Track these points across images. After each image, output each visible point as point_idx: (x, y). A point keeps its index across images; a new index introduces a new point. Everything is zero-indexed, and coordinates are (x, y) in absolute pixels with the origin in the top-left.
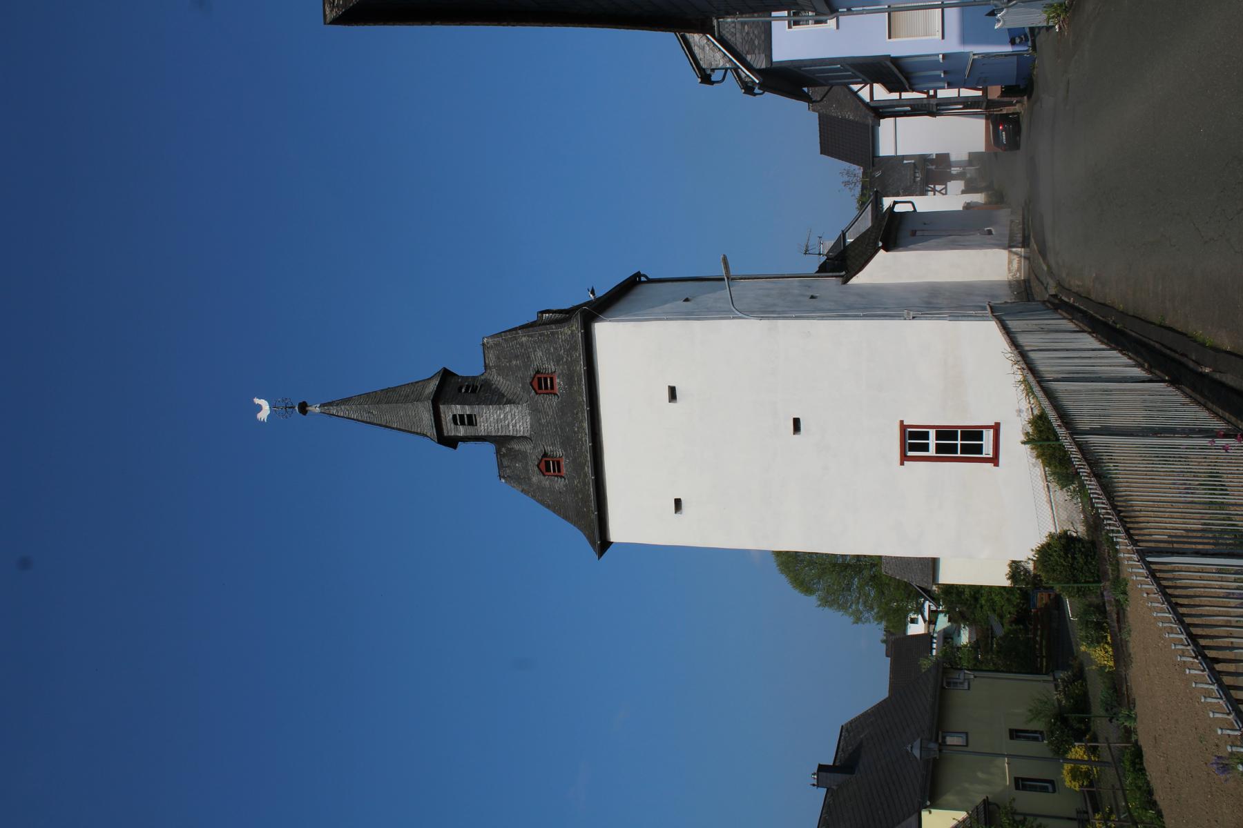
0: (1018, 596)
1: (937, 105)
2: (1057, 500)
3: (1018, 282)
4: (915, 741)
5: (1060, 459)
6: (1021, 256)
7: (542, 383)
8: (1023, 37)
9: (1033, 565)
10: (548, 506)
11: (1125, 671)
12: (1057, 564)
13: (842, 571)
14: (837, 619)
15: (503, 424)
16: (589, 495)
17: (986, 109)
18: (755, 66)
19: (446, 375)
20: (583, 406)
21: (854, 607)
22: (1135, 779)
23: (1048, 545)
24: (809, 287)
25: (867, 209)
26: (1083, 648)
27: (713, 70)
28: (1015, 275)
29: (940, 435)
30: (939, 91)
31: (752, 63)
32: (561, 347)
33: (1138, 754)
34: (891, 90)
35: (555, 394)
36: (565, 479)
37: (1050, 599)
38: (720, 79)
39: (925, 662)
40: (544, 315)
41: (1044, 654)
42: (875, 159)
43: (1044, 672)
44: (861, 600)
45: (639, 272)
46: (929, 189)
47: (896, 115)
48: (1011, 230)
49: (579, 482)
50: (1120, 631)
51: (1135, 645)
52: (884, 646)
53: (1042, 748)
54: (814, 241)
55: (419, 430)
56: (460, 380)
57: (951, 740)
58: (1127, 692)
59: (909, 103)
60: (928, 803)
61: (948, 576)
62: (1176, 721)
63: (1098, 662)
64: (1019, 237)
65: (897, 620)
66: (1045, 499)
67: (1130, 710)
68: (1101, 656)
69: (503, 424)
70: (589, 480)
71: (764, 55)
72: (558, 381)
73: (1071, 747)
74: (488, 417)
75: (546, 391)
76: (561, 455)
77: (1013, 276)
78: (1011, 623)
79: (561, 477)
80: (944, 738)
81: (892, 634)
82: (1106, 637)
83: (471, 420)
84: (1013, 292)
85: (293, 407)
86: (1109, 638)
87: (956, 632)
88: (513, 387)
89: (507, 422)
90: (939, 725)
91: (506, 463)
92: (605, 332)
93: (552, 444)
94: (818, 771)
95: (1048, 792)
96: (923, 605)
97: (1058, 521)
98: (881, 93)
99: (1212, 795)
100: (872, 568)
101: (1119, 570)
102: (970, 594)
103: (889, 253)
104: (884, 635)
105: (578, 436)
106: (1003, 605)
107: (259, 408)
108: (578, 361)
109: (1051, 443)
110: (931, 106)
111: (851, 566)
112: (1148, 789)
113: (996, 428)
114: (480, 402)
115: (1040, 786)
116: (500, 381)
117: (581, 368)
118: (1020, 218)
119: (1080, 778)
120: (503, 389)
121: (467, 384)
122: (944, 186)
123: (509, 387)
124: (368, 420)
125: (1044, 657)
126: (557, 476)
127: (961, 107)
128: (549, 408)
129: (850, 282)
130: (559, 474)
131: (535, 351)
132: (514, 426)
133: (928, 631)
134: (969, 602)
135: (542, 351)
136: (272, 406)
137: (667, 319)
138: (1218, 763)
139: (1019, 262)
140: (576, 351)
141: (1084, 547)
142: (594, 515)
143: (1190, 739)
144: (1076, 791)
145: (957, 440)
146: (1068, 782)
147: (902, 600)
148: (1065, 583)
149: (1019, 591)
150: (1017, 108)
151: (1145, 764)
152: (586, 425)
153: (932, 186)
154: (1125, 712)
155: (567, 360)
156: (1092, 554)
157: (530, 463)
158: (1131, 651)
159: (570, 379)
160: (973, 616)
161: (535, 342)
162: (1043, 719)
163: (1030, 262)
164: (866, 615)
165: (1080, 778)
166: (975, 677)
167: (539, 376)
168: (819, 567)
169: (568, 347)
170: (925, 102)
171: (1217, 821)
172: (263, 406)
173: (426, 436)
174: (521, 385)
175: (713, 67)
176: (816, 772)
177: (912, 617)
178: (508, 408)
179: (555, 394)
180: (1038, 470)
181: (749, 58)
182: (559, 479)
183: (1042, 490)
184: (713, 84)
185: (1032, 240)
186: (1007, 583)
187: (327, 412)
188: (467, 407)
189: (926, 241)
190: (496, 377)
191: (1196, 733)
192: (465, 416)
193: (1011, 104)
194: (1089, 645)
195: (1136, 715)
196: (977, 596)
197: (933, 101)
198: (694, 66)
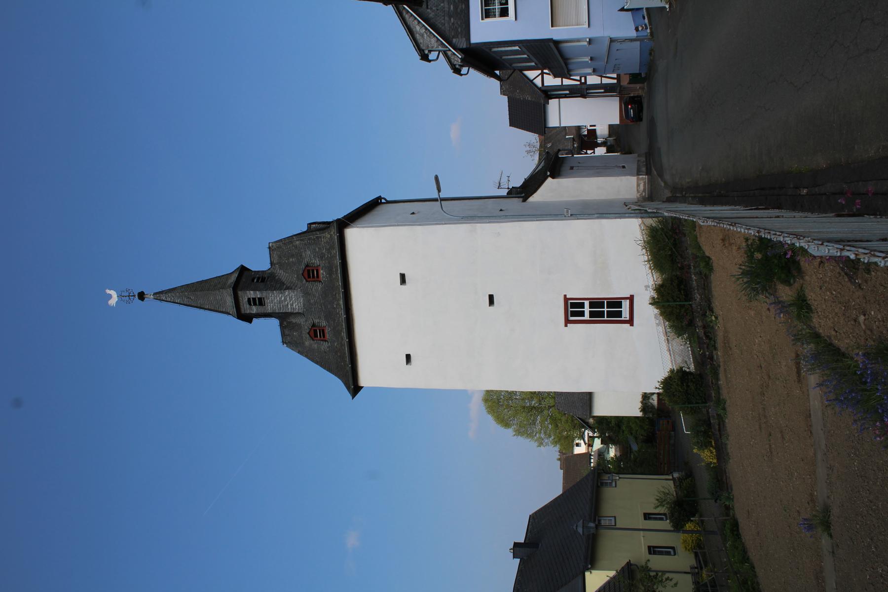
4: (579, 521)
7: (310, 274)
8: (643, 26)
10: (317, 363)
14: (526, 444)
15: (284, 304)
16: (345, 353)
19: (243, 270)
21: (538, 436)
26: (695, 451)
27: (430, 51)
29: (592, 305)
30: (588, 77)
32: (323, 247)
33: (735, 526)
34: (555, 76)
35: (320, 281)
45: (380, 196)
47: (559, 97)
50: (721, 437)
51: (732, 445)
55: (224, 310)
56: (253, 273)
58: (726, 480)
60: (590, 566)
63: (706, 460)
65: (567, 443)
66: (666, 349)
68: (707, 456)
70: (344, 343)
72: (322, 271)
77: (640, 195)
79: (325, 341)
81: (564, 454)
82: (711, 442)
83: (261, 302)
85: (134, 296)
86: (713, 442)
87: (607, 450)
88: (290, 277)
91: (287, 332)
93: (319, 318)
94: (514, 547)
95: (671, 555)
100: (549, 409)
104: (559, 455)
108: (336, 257)
109: (671, 304)
111: (535, 408)
113: (631, 299)
115: (665, 551)
117: (338, 261)
120: (284, 279)
122: (593, 151)
123: (288, 278)
124: (188, 304)
126: (322, 340)
127: (603, 91)
128: (316, 292)
130: (324, 339)
132: (292, 305)
134: (614, 429)
136: (120, 296)
138: (805, 524)
141: (694, 378)
147: (570, 430)
149: (647, 420)
152: (341, 302)
153: (585, 151)
154: (725, 494)
155: (328, 256)
156: (700, 383)
159: (330, 270)
166: (620, 478)
167: (308, 268)
169: (328, 247)
170: (579, 87)
171: (798, 569)
172: (113, 295)
176: (512, 547)
179: (320, 281)
182: (324, 343)
186: (640, 414)
190: (278, 270)
195: (733, 496)
198: (416, 48)
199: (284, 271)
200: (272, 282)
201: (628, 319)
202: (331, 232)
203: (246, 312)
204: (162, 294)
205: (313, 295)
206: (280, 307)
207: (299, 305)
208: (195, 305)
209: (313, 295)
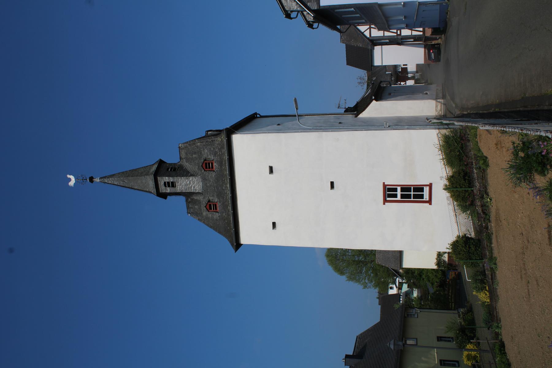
0: (440, 274)
1: (401, 39)
2: (460, 221)
5: (462, 198)
6: (442, 103)
7: (207, 166)
9: (447, 259)
10: (211, 227)
11: (495, 304)
12: (461, 250)
14: (356, 287)
16: (230, 221)
17: (424, 42)
18: (311, 8)
20: (227, 176)
21: (363, 281)
22: (501, 358)
23: (457, 241)
27: (292, 11)
28: (439, 113)
29: (403, 190)
31: (310, 7)
32: (216, 147)
33: (502, 345)
36: (219, 213)
37: (455, 275)
38: (295, 16)
39: (397, 306)
40: (209, 132)
41: (453, 301)
43: (453, 309)
45: (256, 113)
46: (398, 84)
47: (382, 44)
49: (226, 215)
51: (501, 290)
52: (378, 300)
53: (453, 344)
54: (342, 102)
56: (168, 165)
57: (409, 342)
58: (496, 314)
59: (388, 38)
61: (409, 263)
62: (524, 327)
64: (441, 95)
65: (383, 287)
66: (455, 221)
67: (498, 324)
68: (483, 297)
69: (189, 186)
70: (230, 213)
71: (316, 3)
72: (215, 164)
73: (467, 344)
74: (181, 183)
77: (438, 113)
78: (437, 287)
80: (406, 341)
82: (486, 287)
83: (173, 185)
85: (86, 179)
86: (487, 288)
87: (412, 292)
88: (194, 168)
90: (403, 335)
91: (190, 206)
92: (237, 139)
95: (456, 367)
96: (395, 280)
97: (461, 232)
98: (376, 33)
99: (545, 364)
101: (492, 253)
102: (418, 273)
103: (377, 102)
106: (433, 278)
107: (70, 180)
108: (225, 154)
109: (458, 189)
110: (398, 40)
111: (362, 261)
112: (508, 363)
113: (430, 186)
115: (452, 364)
116: (187, 166)
117: (226, 157)
118: (441, 88)
119: (471, 359)
120: (189, 169)
122: (405, 83)
124: (123, 185)
125: (453, 302)
126: (215, 212)
127: (412, 40)
129: (359, 117)
130: (216, 211)
131: (204, 150)
132: (194, 187)
133: (399, 292)
135: (207, 150)
137: (268, 133)
140: (224, 148)
141: (474, 242)
143: (532, 335)
144: (469, 366)
145: (413, 194)
146: (465, 361)
148: (465, 260)
150: (439, 41)
151: (506, 351)
152: (228, 186)
153: (399, 83)
154: (495, 324)
155: (219, 153)
156: (479, 245)
157: (202, 206)
158: (499, 294)
159: (221, 164)
160: (419, 284)
161: (204, 145)
162: (453, 331)
163: (446, 106)
164: (369, 285)
165: (471, 359)
166: (420, 311)
167: (205, 162)
168: (347, 262)
169: (220, 147)
170: (396, 37)
173: (152, 193)
175: (292, 10)
176: (344, 358)
177: (391, 286)
178: (191, 178)
180: (451, 206)
181: (309, 4)
182: (216, 213)
183: (453, 216)
184: (291, 19)
185: (447, 95)
187: (103, 181)
188: (171, 178)
189: (396, 97)
190: (185, 163)
191: (536, 332)
192: (170, 183)
193: (436, 39)
194: (477, 292)
195: (501, 325)
196: (421, 274)
197: (399, 37)
200: (181, 171)
201: (428, 200)
202: (221, 137)
203: (163, 192)
205: (209, 180)
207: (199, 186)
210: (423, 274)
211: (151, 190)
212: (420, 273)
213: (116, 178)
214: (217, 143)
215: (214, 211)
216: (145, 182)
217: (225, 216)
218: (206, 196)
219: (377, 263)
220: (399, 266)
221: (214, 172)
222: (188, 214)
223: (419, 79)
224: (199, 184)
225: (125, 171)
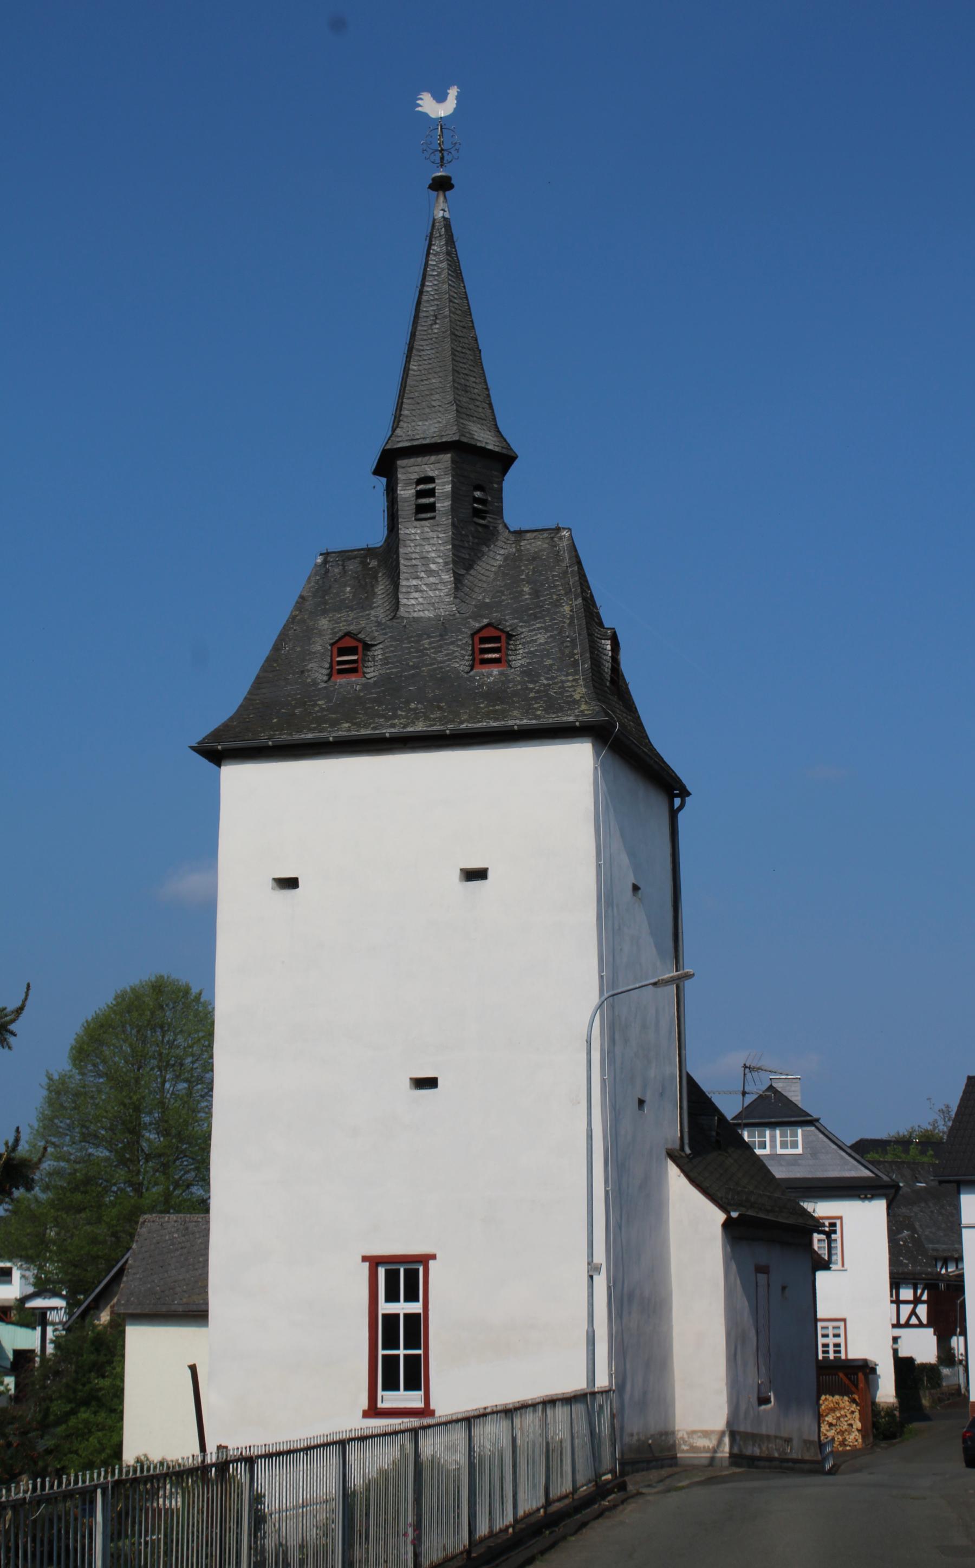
3: (673, 1447)
6: (715, 1451)
10: (277, 648)
13: (123, 1123)
15: (420, 568)
16: (300, 731)
19: (505, 460)
20: (452, 721)
24: (661, 1095)
25: (863, 1168)
28: (685, 1442)
32: (553, 678)
36: (326, 682)
42: (955, 1185)
44: (62, 1164)
45: (689, 794)
46: (919, 1292)
48: (768, 1437)
49: (322, 710)
55: (405, 412)
56: (495, 486)
64: (753, 1450)
74: (432, 542)
75: (477, 651)
76: (368, 676)
77: (682, 1438)
79: (330, 675)
83: (424, 510)
84: (652, 1436)
88: (485, 585)
89: (423, 575)
91: (352, 566)
93: (386, 658)
100: (131, 1184)
105: (401, 709)
107: (440, 98)
114: (457, 527)
117: (517, 721)
120: (480, 567)
121: (489, 499)
123: (484, 578)
124: (422, 314)
126: (331, 667)
128: (447, 655)
129: (669, 1160)
130: (335, 672)
131: (546, 629)
134: (80, 1387)
139: (705, 1449)
142: (265, 739)
145: (398, 1356)
153: (925, 1297)
155: (531, 690)
157: (352, 614)
159: (497, 695)
161: (561, 631)
169: (551, 693)
174: (487, 600)
178: (447, 577)
188: (448, 503)
190: (502, 552)
192: (432, 500)
196: (94, 1403)
199: (500, 566)
200: (473, 537)
201: (380, 1405)
202: (586, 703)
203: (400, 470)
204: (447, 244)
205: (441, 646)
206: (411, 559)
207: (418, 608)
208: (418, 336)
209: (441, 646)
210: (95, 1413)
211: (405, 425)
212: (98, 1399)
213: (446, 286)
214: (568, 681)
215: (334, 664)
216: (434, 403)
217: (315, 705)
218: (385, 634)
219: (141, 1220)
220: (130, 1311)
221: (467, 669)
222: (321, 554)
223: (939, 1385)
224: (426, 606)
225: (472, 321)
